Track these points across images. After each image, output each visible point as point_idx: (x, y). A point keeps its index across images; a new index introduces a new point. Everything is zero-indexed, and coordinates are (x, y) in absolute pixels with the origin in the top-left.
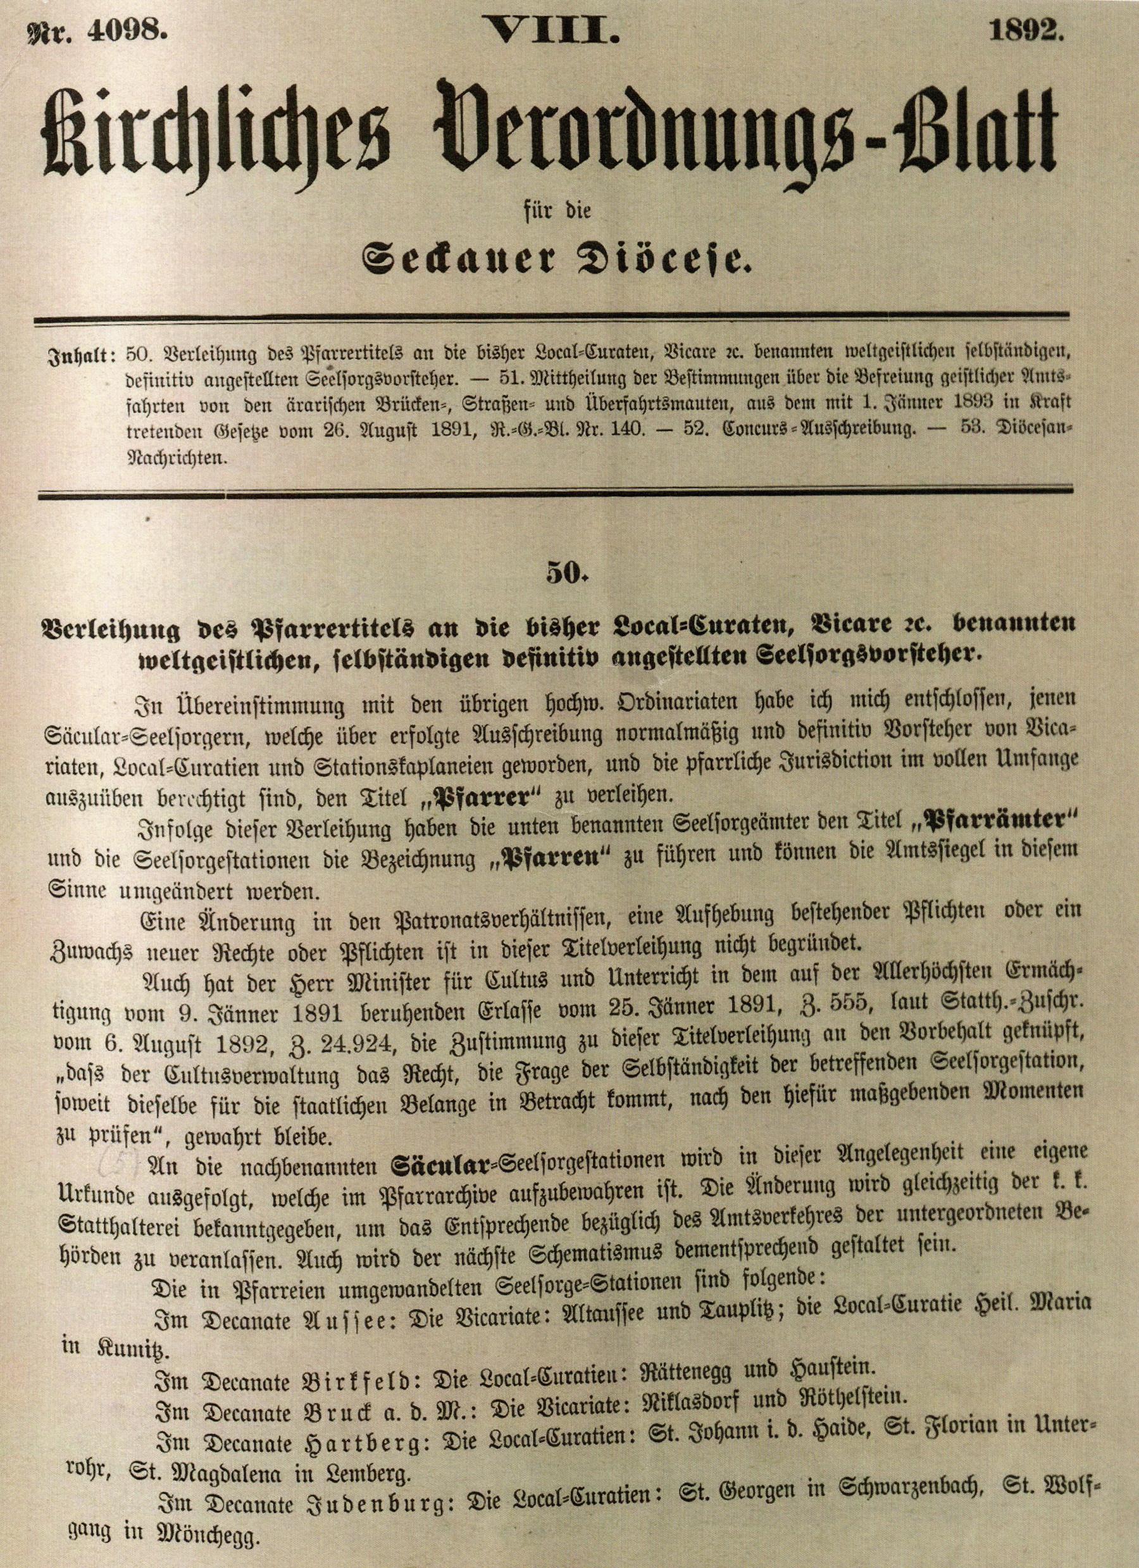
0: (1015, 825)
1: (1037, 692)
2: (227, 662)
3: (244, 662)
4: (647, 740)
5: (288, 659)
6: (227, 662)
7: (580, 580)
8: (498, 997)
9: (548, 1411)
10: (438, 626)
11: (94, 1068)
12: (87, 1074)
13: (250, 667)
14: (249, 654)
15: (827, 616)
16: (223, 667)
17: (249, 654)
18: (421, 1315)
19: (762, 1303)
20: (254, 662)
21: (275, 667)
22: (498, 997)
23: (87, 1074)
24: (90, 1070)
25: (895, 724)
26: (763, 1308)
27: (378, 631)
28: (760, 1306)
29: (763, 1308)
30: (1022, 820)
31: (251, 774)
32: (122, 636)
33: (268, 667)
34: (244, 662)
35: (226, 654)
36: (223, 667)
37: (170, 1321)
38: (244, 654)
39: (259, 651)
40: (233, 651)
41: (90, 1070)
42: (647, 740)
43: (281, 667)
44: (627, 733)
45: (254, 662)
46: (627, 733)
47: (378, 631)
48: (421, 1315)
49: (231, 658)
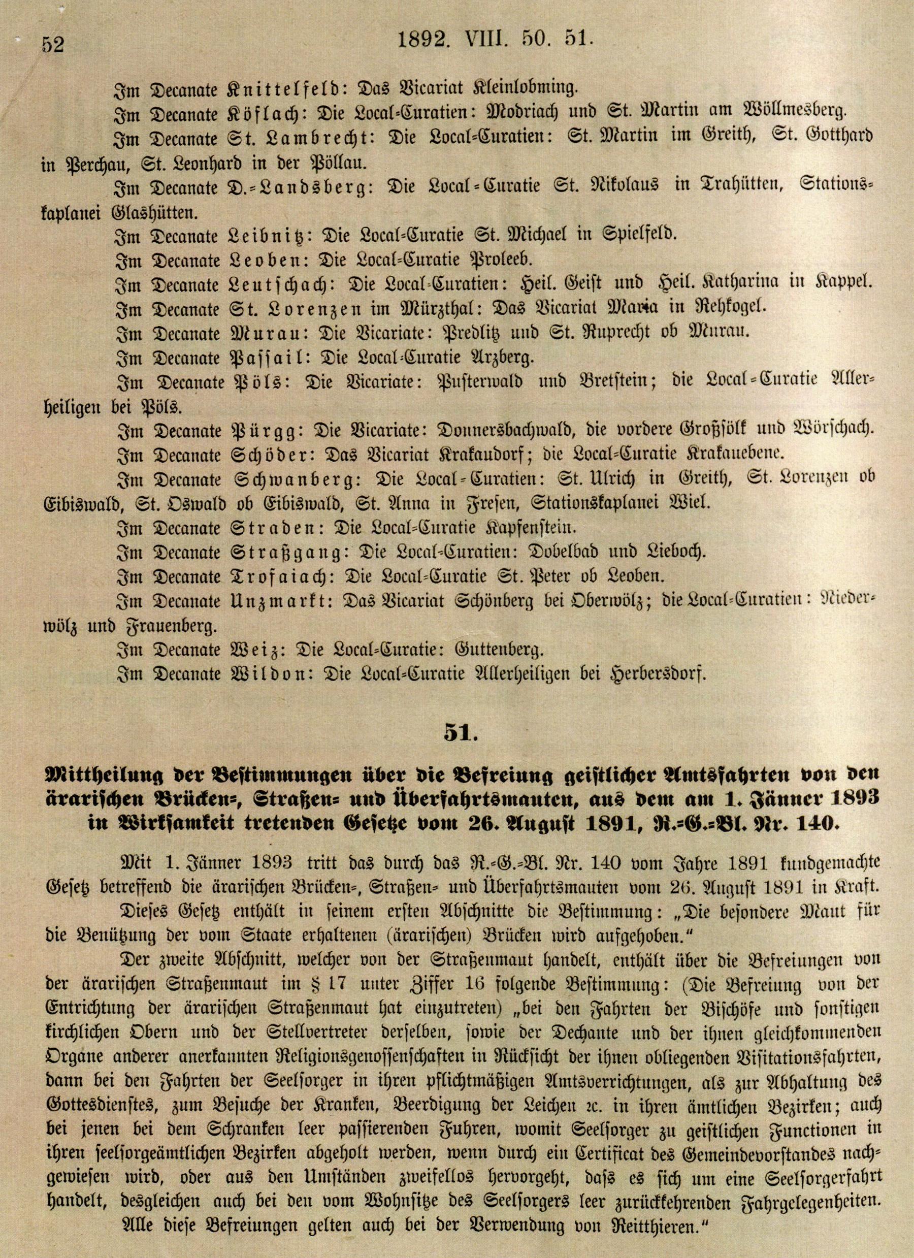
0: (280, 780)
1: (87, 1124)
2: (592, 776)
3: (605, 777)
4: (499, 1231)
5: (639, 774)
6: (592, 776)
7: (493, 829)
8: (224, 1117)
9: (376, 458)
10: (597, 798)
11: (607, 1174)
12: (602, 1178)
13: (609, 780)
14: (609, 770)
15: (64, 769)
16: (589, 780)
17: (609, 770)
18: (315, 379)
19: (490, 328)
20: (612, 777)
21: (628, 780)
22: (224, 1117)
23: (602, 1178)
24: (604, 1175)
25: (365, 329)
26: (491, 332)
27: (550, 801)
28: (488, 330)
29: (491, 332)
30: (285, 776)
31: (243, 916)
32: (463, 804)
33: (623, 780)
34: (605, 777)
35: (591, 770)
36: (589, 780)
37: (128, 263)
38: (604, 770)
39: (616, 768)
40: (596, 768)
41: (604, 1175)
42: (499, 1231)
43: (633, 781)
44: (373, 1056)
45: (612, 777)
46: (373, 1056)
47: (550, 801)
48: (315, 379)
49: (595, 774)
